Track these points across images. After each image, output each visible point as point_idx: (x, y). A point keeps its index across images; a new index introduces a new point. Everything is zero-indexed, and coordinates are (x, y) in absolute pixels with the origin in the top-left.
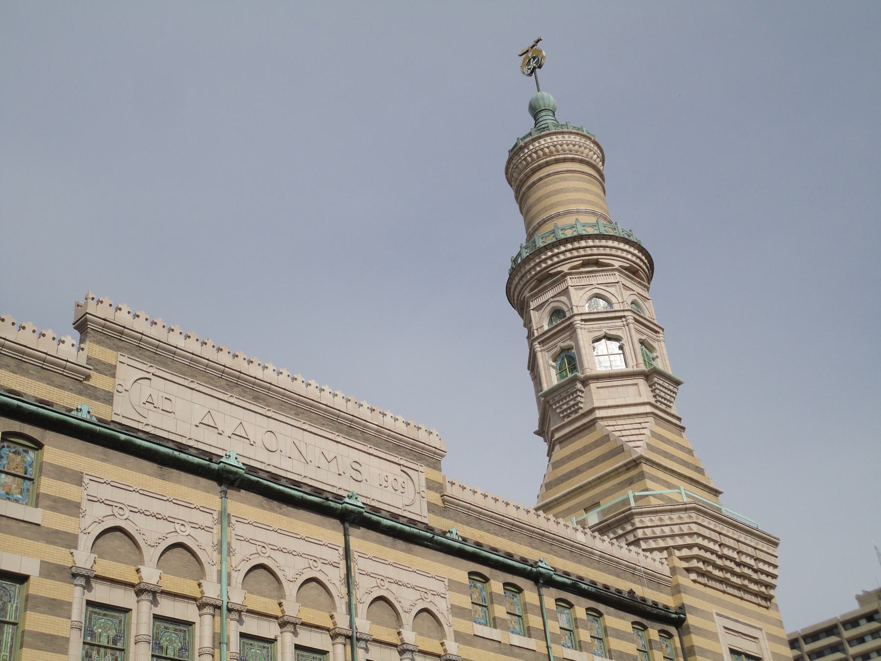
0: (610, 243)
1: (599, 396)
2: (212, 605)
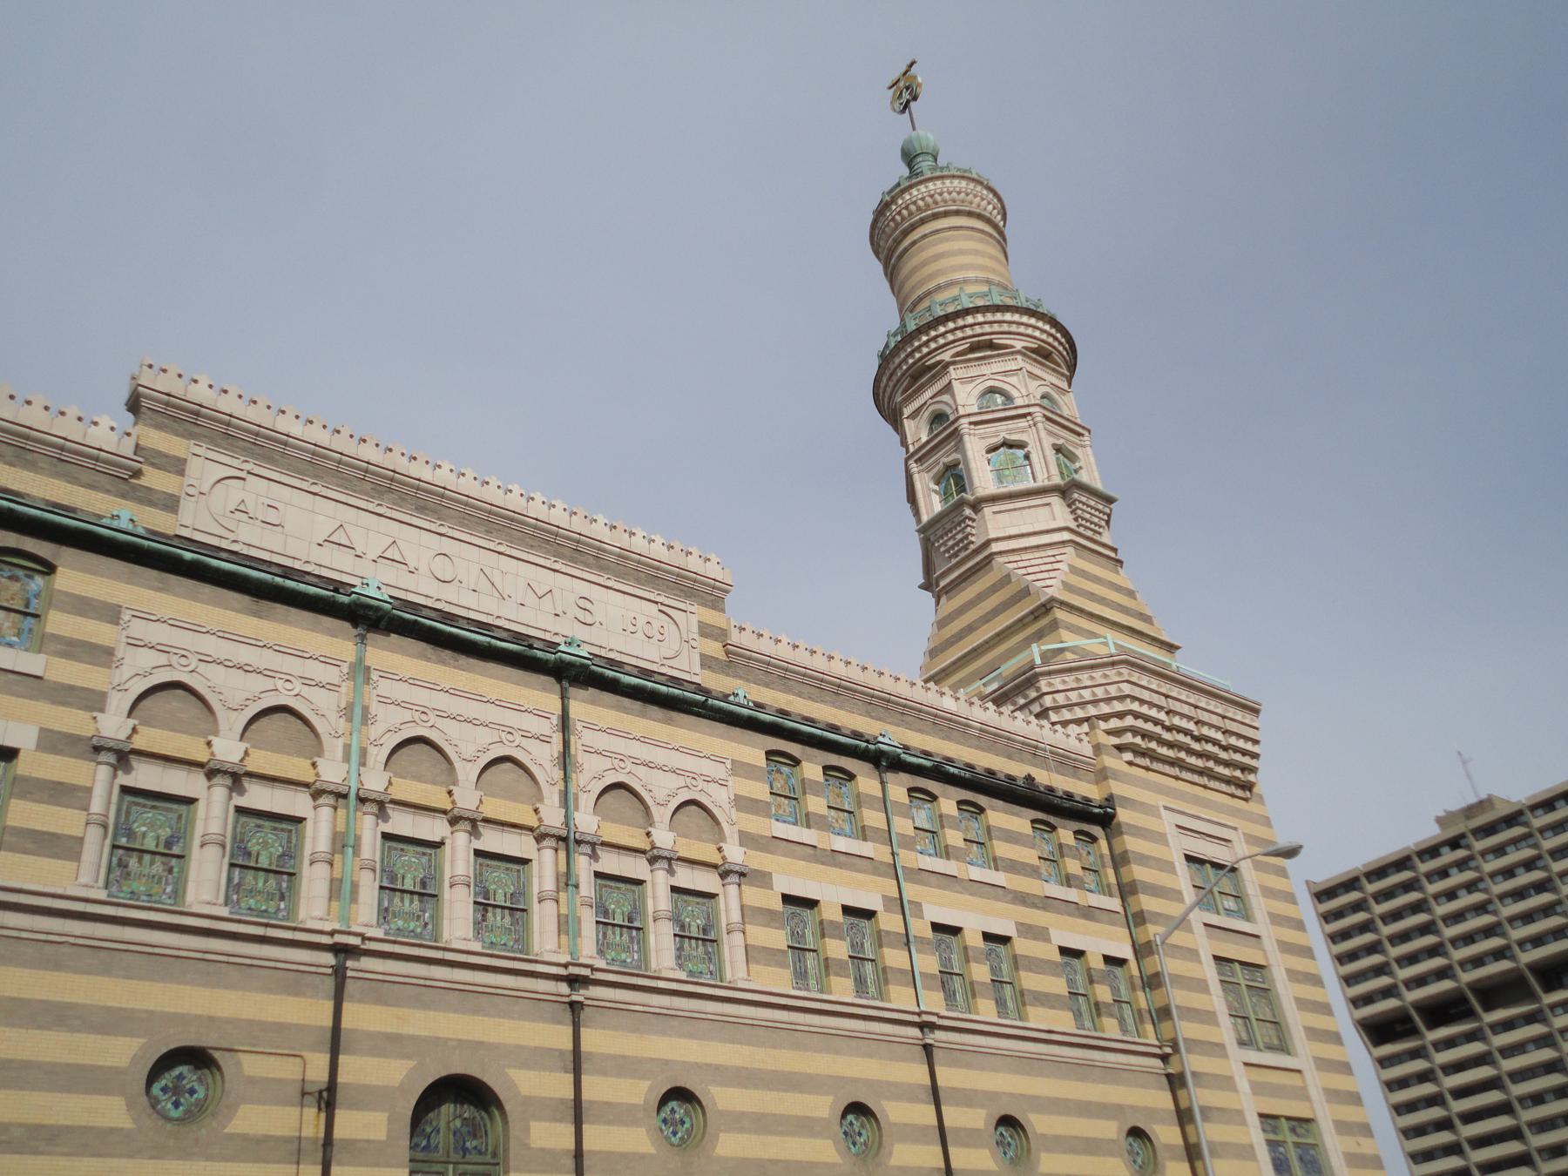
0: (1008, 316)
1: (995, 524)
2: (331, 792)
